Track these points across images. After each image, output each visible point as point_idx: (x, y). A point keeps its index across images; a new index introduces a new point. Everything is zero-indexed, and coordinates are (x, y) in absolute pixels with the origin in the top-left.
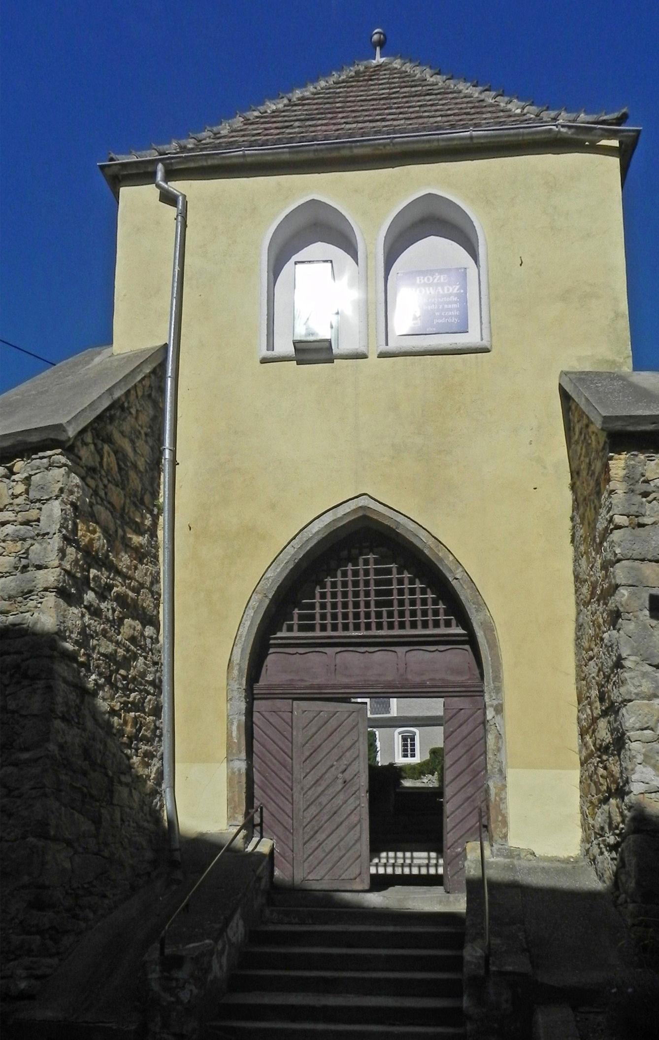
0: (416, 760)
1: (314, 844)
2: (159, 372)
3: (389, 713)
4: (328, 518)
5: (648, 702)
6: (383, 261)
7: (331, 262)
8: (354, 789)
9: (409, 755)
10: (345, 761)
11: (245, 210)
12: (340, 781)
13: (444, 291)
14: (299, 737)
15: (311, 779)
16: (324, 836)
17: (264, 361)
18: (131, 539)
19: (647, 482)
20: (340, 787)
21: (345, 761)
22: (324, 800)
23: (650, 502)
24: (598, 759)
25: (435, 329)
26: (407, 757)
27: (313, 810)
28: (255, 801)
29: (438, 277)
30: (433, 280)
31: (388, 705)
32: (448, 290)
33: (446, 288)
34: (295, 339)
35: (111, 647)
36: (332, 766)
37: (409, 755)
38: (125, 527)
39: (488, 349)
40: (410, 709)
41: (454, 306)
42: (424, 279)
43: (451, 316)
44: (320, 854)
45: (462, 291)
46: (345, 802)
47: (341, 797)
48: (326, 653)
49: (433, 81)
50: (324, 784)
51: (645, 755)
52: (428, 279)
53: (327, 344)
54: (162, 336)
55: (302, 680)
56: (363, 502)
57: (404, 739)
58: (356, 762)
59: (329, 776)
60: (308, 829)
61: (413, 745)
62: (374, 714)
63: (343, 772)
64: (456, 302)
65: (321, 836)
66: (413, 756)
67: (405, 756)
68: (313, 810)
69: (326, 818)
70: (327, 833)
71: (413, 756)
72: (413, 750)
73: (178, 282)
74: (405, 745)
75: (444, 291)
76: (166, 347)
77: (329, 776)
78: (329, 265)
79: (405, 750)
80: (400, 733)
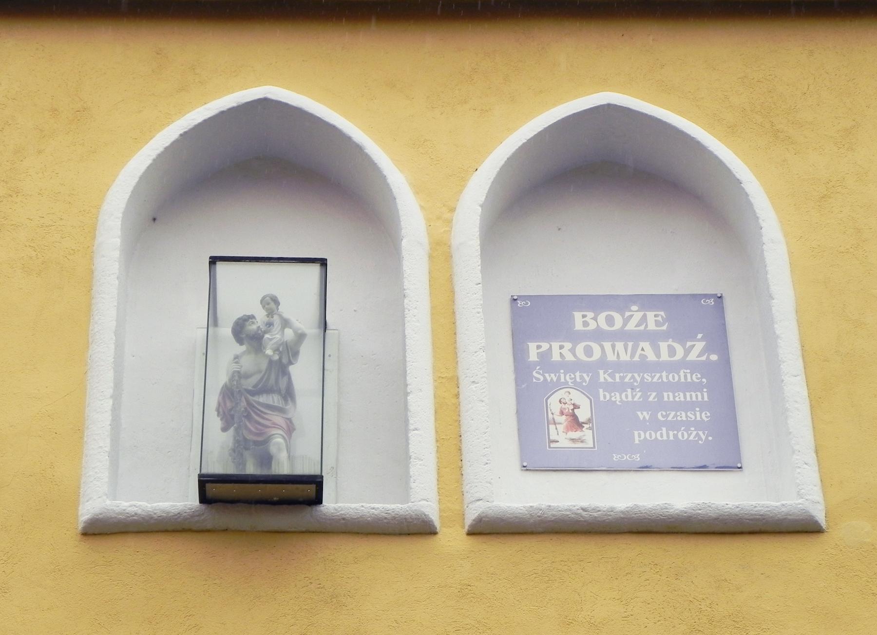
6: (478, 222)
7: (323, 262)
13: (658, 355)
25: (637, 457)
28: (282, 392)
29: (638, 316)
30: (625, 324)
32: (672, 351)
33: (663, 346)
34: (204, 471)
39: (816, 523)
41: (693, 396)
42: (595, 319)
43: (688, 424)
45: (714, 357)
48: (477, 285)
52: (610, 321)
53: (311, 489)
64: (702, 406)
75: (658, 355)
78: (316, 269)
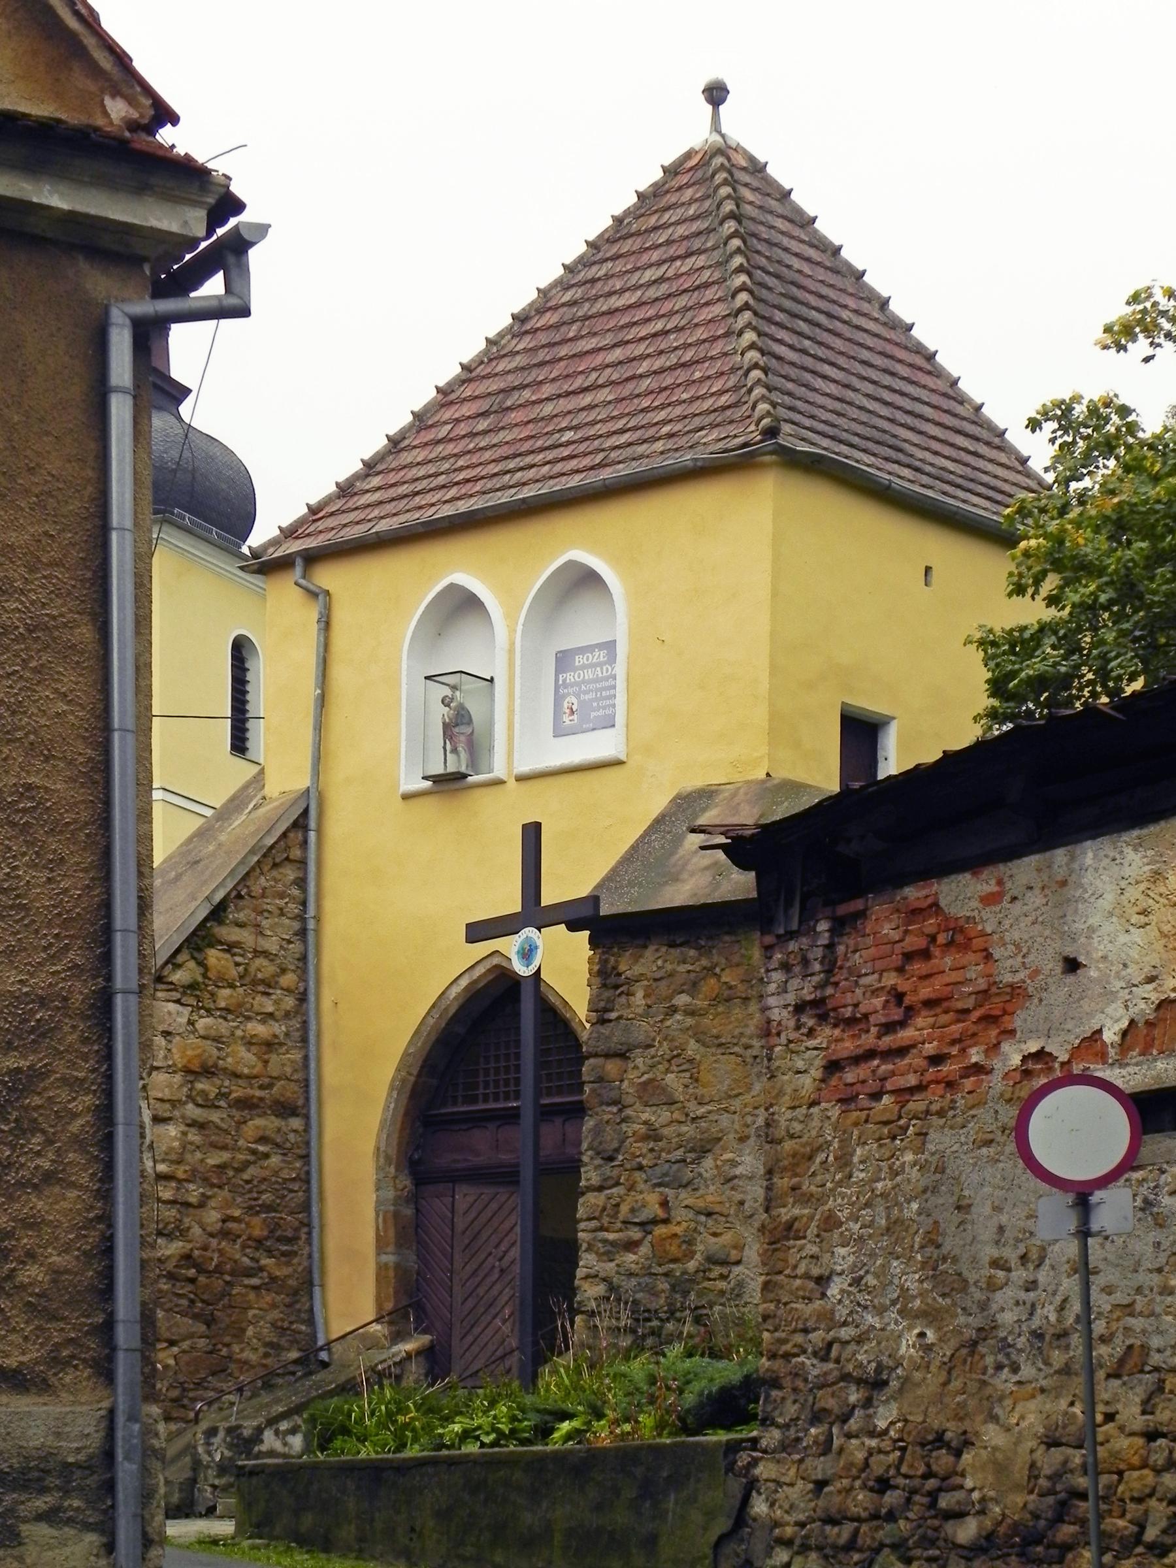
1: (470, 1338)
2: (301, 823)
4: (464, 982)
5: (277, 1122)
8: (510, 1277)
10: (503, 1248)
12: (497, 1271)
14: (460, 1224)
15: (469, 1268)
16: (479, 1330)
17: (406, 797)
18: (1163, 548)
19: (619, 975)
20: (497, 1276)
21: (503, 1248)
22: (481, 1291)
23: (620, 995)
24: (288, 1145)
27: (470, 1303)
35: (225, 1156)
36: (490, 1254)
44: (475, 1349)
46: (501, 1293)
47: (498, 1287)
50: (481, 1274)
51: (589, 1244)
54: (303, 782)
55: (466, 1160)
56: (496, 960)
58: (514, 1249)
59: (488, 1265)
60: (464, 1324)
63: (500, 1260)
65: (477, 1331)
68: (470, 1303)
69: (482, 1310)
70: (483, 1325)
76: (308, 790)
77: (488, 1265)
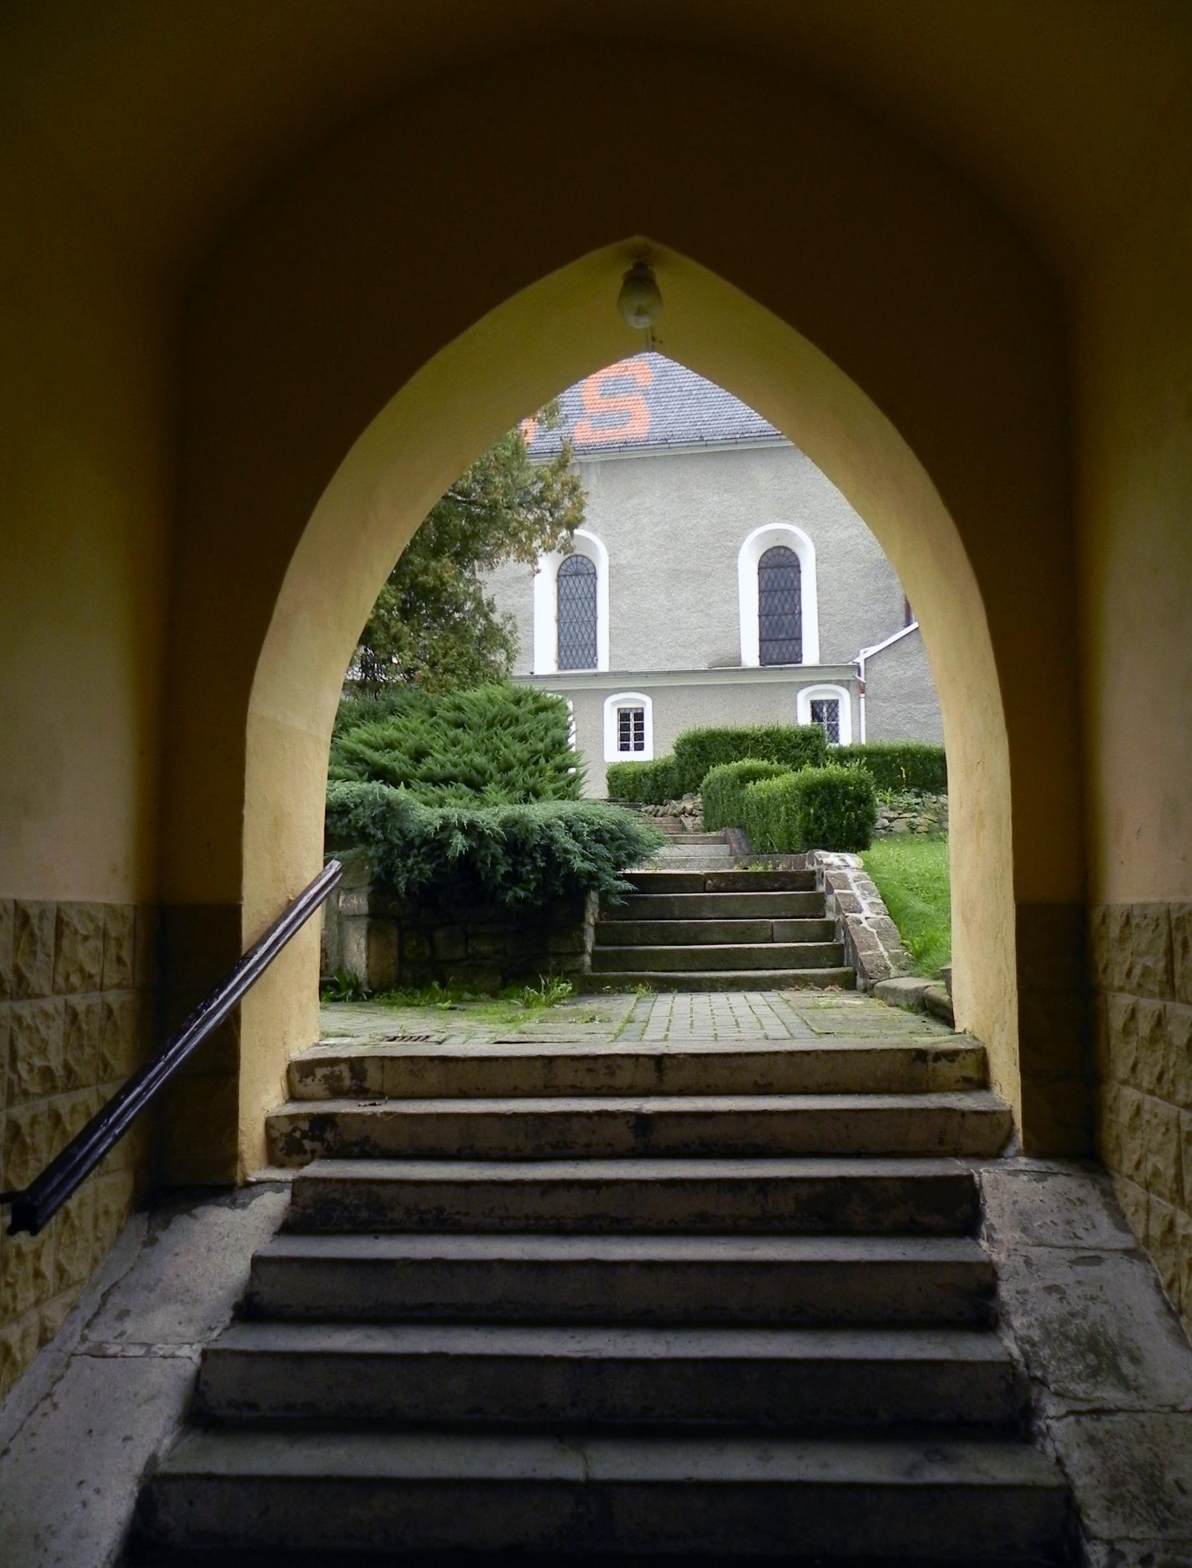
0: (646, 756)
3: (595, 666)
9: (632, 716)
11: (67, 1502)
26: (628, 749)
31: (592, 652)
37: (632, 716)
38: (243, 953)
40: (634, 658)
49: (339, 773)
57: (624, 716)
61: (639, 727)
62: (565, 668)
66: (639, 747)
67: (624, 748)
71: (639, 747)
72: (640, 737)
73: (105, 1141)
74: (624, 728)
79: (624, 738)
80: (614, 703)
